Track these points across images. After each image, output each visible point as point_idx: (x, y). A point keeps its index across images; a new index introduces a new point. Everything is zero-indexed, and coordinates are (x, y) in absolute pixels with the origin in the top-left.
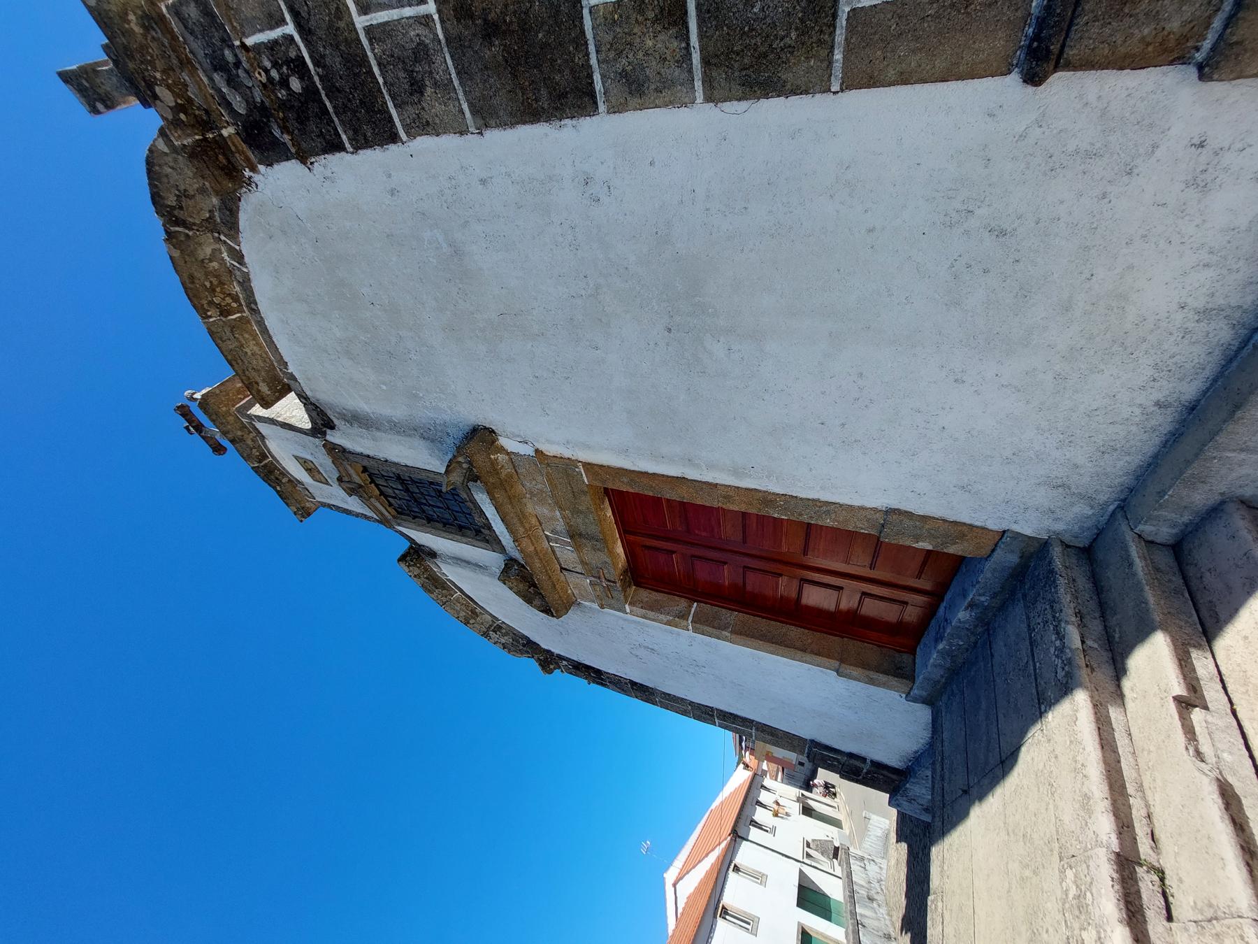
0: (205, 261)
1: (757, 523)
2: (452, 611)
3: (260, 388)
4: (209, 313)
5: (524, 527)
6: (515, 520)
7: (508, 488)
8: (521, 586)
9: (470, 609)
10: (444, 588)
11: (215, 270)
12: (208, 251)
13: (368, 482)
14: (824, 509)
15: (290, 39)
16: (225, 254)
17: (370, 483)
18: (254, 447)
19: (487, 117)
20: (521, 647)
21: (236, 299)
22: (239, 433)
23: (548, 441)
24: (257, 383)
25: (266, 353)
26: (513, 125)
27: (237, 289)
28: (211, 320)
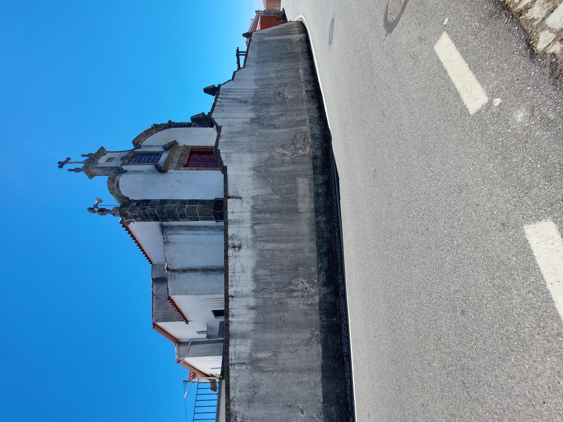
12: (154, 131)
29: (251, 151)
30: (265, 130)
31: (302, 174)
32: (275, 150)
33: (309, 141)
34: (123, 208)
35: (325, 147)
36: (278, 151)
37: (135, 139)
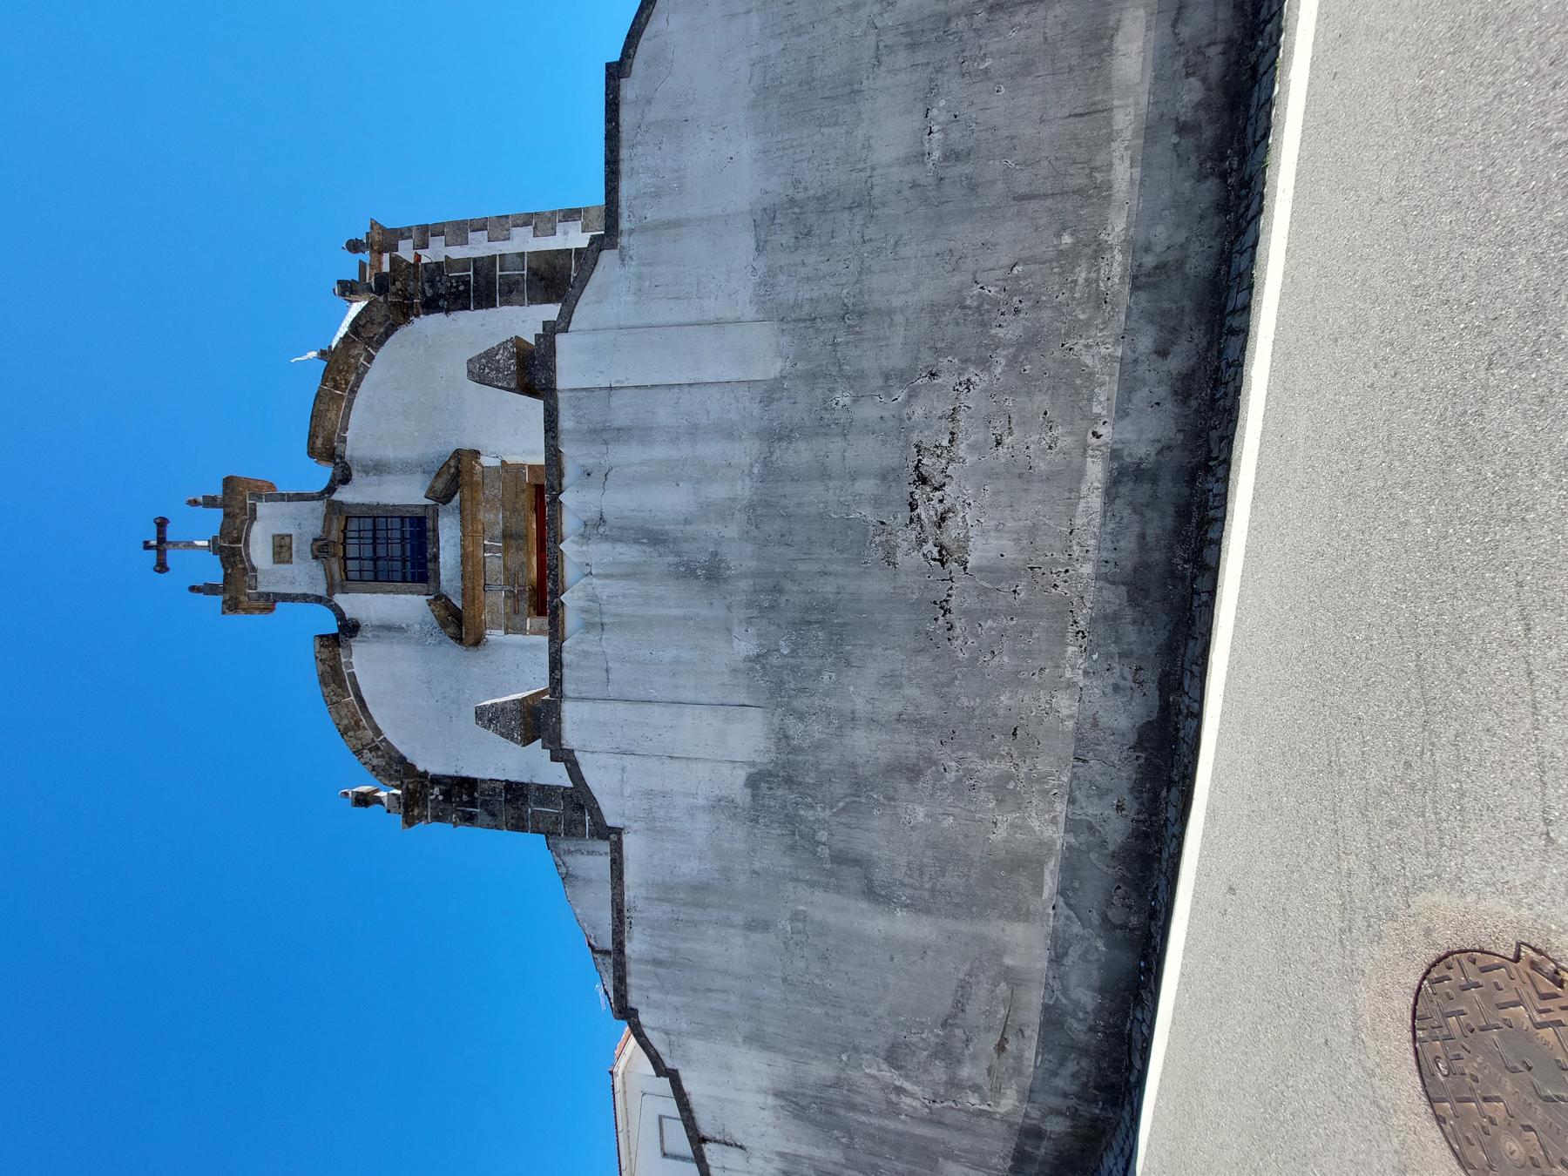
2: (336, 716)
6: (469, 517)
8: (442, 612)
10: (340, 686)
12: (356, 352)
15: (469, 275)
17: (342, 544)
19: (532, 301)
22: (237, 511)
23: (512, 454)
24: (317, 437)
26: (541, 304)
27: (353, 378)
29: (757, 1039)
30: (819, 895)
31: (965, 1157)
32: (861, 1065)
33: (1027, 1054)
34: (412, 811)
35: (1095, 1119)
36: (874, 1072)
37: (312, 436)
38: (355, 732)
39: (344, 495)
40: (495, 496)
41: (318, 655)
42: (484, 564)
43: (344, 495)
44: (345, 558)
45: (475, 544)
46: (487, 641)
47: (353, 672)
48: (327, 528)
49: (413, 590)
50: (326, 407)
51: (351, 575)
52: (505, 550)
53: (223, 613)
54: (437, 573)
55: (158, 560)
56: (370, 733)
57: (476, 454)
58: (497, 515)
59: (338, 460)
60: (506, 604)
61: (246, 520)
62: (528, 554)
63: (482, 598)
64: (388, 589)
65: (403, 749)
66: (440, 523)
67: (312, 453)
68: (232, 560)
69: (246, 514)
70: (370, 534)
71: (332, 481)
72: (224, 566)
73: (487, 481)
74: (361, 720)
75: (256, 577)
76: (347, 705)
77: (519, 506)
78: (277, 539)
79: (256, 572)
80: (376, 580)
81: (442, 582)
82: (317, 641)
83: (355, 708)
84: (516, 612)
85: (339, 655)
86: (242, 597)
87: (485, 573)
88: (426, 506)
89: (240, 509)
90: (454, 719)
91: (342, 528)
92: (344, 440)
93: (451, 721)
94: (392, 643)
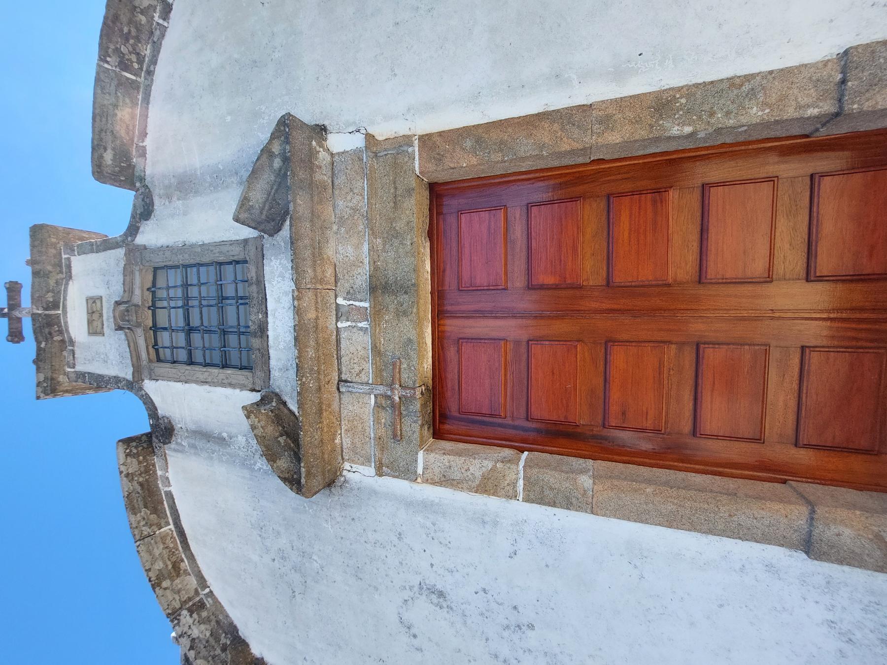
0: (138, 10)
1: (630, 230)
3: (105, 155)
4: (108, 59)
5: (315, 271)
6: (308, 253)
7: (316, 198)
8: (270, 429)
9: (174, 559)
11: (141, 24)
13: (147, 305)
14: (746, 87)
16: (158, 14)
17: (149, 308)
18: (53, 291)
20: (218, 651)
21: (141, 61)
22: (49, 268)
23: (388, 118)
24: (105, 149)
25: (134, 126)
28: (106, 66)
37: (97, 147)
38: (172, 581)
39: (149, 236)
40: (355, 210)
41: (123, 468)
42: (338, 341)
43: (149, 236)
44: (155, 328)
45: (320, 305)
46: (345, 481)
47: (170, 491)
48: (128, 288)
49: (234, 382)
50: (113, 100)
51: (166, 354)
52: (376, 315)
53: (38, 398)
54: (266, 357)
55: (10, 329)
56: (193, 581)
57: (321, 131)
58: (357, 247)
59: (138, 185)
60: (377, 421)
61: (62, 279)
62: (419, 325)
63: (335, 406)
64: (202, 377)
65: (237, 615)
66: (266, 268)
67: (99, 172)
68: (47, 330)
69: (61, 272)
70: (179, 293)
71: (133, 217)
72: (36, 339)
73: (340, 180)
74: (182, 561)
75: (73, 352)
76: (163, 538)
77: (400, 225)
78: (90, 302)
79: (73, 346)
80: (191, 362)
81: (272, 372)
82: (121, 448)
83: (175, 542)
84: (397, 437)
85: (154, 465)
86: (61, 376)
87: (339, 358)
88: (246, 241)
89: (54, 266)
90: (298, 597)
91: (149, 285)
92: (143, 153)
93: (294, 596)
94: (212, 458)
